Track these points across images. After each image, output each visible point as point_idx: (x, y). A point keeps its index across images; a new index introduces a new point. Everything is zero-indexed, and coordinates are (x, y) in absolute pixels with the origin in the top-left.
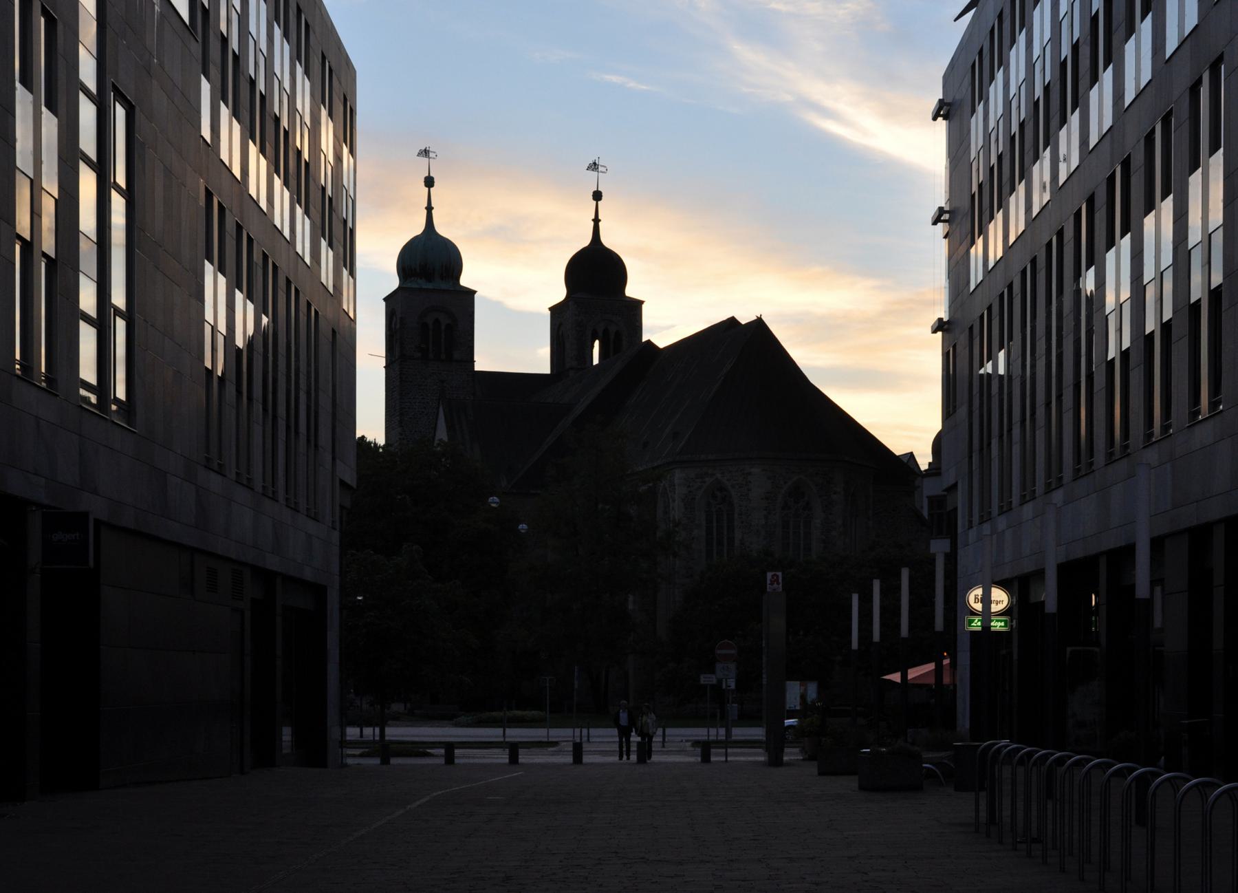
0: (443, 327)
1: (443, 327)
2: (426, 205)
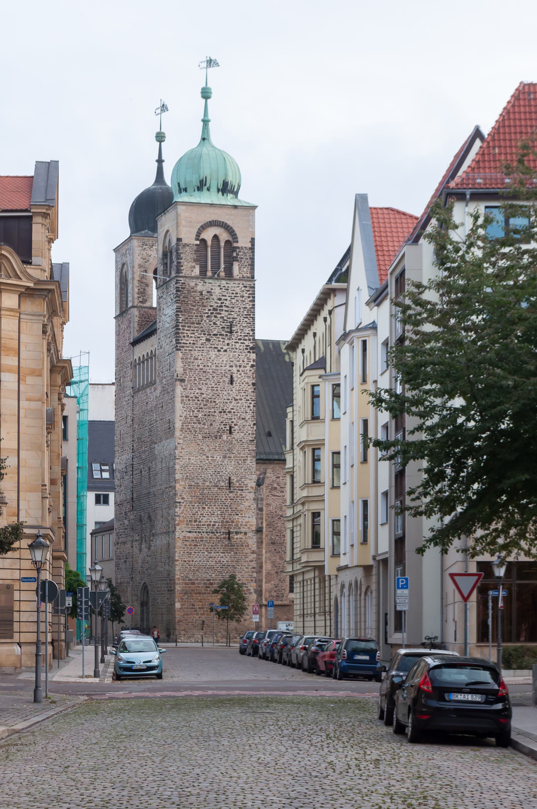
0: (222, 244)
1: (222, 244)
2: (202, 117)
